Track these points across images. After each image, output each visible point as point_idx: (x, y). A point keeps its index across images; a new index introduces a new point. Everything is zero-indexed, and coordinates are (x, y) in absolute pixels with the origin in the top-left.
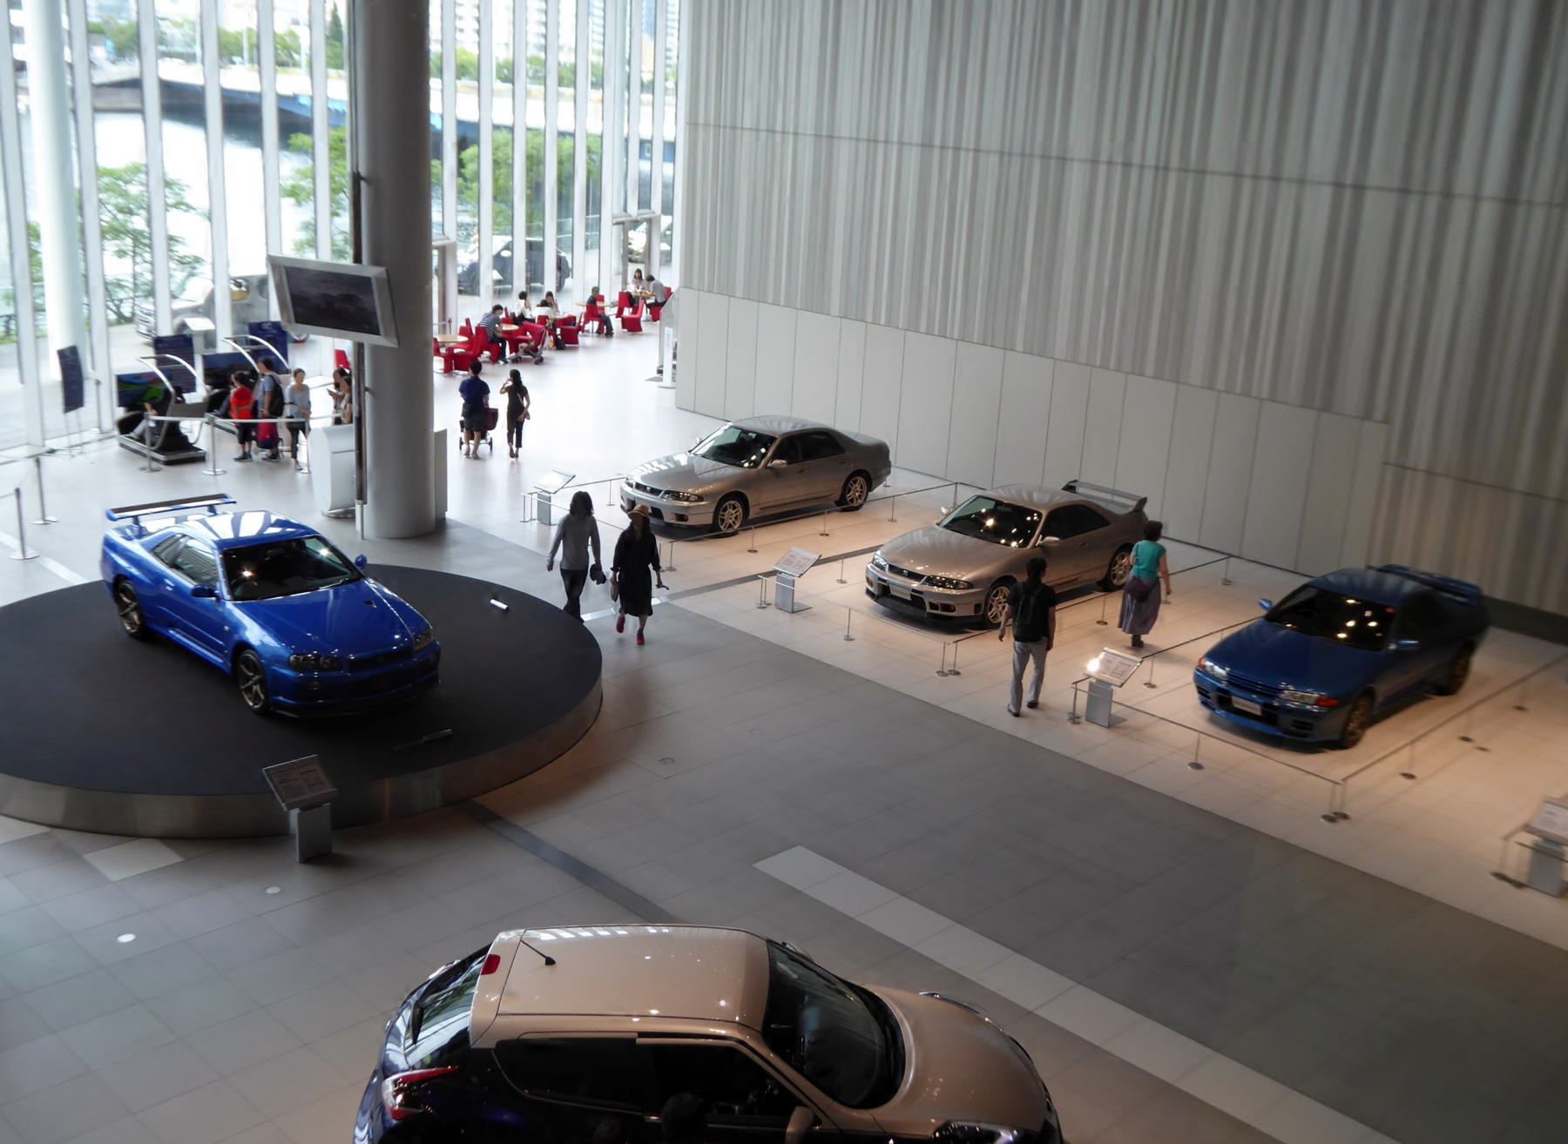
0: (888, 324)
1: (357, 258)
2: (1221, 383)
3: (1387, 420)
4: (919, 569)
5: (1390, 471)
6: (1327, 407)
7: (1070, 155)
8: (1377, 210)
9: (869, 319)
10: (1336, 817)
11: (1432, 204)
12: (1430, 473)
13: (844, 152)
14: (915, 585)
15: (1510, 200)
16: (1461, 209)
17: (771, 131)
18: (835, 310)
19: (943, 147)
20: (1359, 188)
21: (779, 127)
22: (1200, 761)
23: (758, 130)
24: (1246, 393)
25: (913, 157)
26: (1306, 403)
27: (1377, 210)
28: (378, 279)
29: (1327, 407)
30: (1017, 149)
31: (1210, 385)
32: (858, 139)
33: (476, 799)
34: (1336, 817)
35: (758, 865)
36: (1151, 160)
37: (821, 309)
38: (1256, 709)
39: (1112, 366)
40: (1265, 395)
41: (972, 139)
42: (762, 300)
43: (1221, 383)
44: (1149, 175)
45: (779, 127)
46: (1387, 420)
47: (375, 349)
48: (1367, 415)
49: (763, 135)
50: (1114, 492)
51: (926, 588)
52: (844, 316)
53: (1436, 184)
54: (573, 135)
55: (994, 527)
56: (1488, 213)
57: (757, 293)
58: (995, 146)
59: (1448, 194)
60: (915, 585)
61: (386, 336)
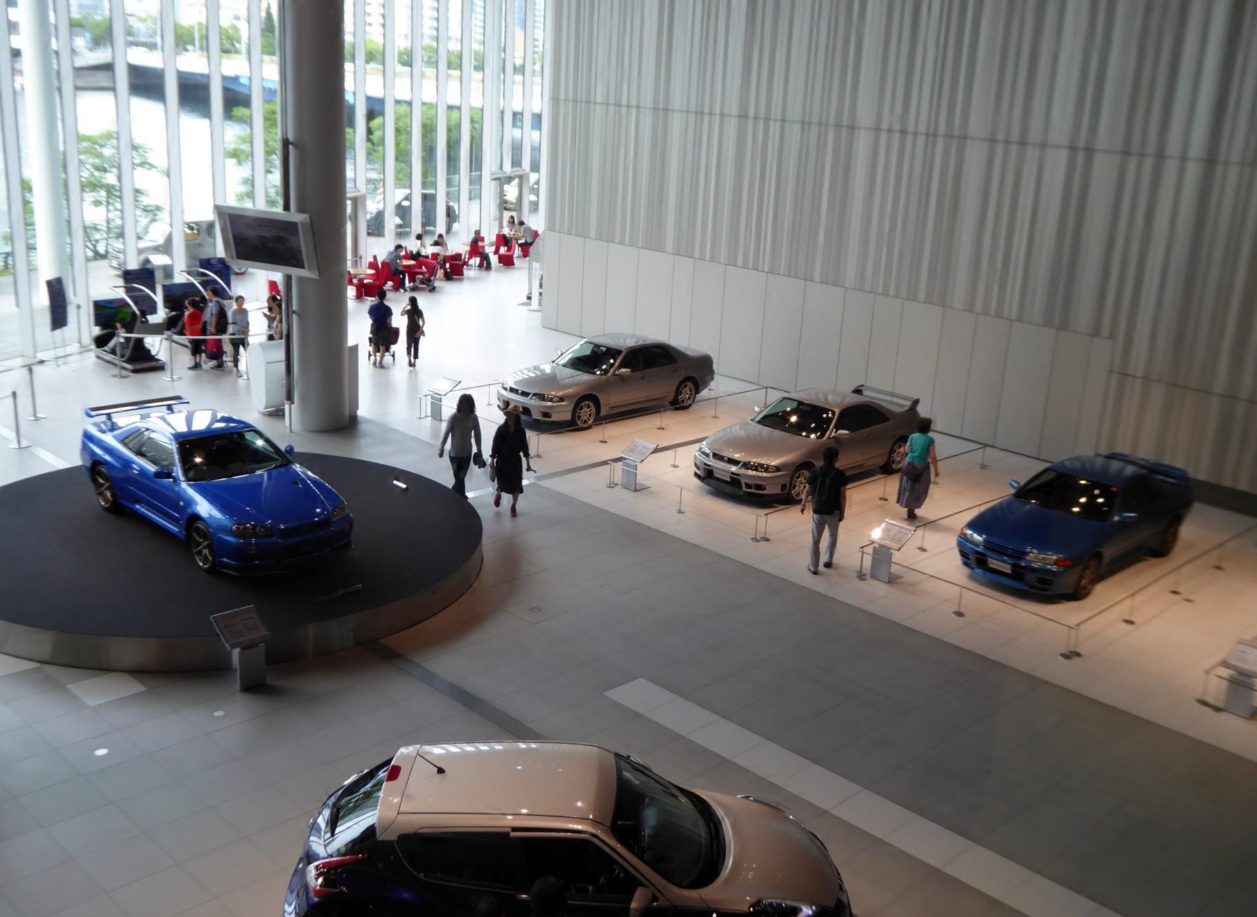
0: (712, 260)
1: (287, 207)
2: (979, 307)
3: (1112, 337)
4: (737, 456)
5: (1114, 377)
6: (1064, 326)
7: (857, 125)
8: (1104, 169)
9: (697, 256)
10: (1071, 655)
11: (1148, 164)
12: (1146, 379)
13: (676, 122)
14: (734, 469)
15: (1210, 160)
16: (1171, 168)
17: (618, 105)
18: (669, 248)
19: (756, 118)
20: (1090, 151)
21: (624, 102)
22: (962, 610)
23: (607, 104)
24: (999, 315)
25: (732, 126)
26: (1047, 323)
27: (1104, 169)
28: (303, 224)
29: (1064, 326)
30: (815, 119)
31: (970, 309)
32: (687, 112)
33: (381, 641)
34: (1071, 655)
35: (607, 694)
36: (922, 128)
37: (658, 247)
38: (1007, 569)
39: (891, 293)
40: (1014, 316)
41: (780, 111)
42: (610, 240)
43: (979, 307)
44: (921, 140)
45: (624, 102)
46: (1112, 337)
47: (301, 280)
48: (1096, 333)
49: (612, 109)
50: (893, 395)
51: (743, 471)
52: (677, 253)
53: (1151, 147)
54: (459, 108)
55: (797, 422)
56: (1193, 171)
57: (607, 235)
58: (798, 117)
59: (1160, 156)
60: (734, 469)
61: (309, 269)
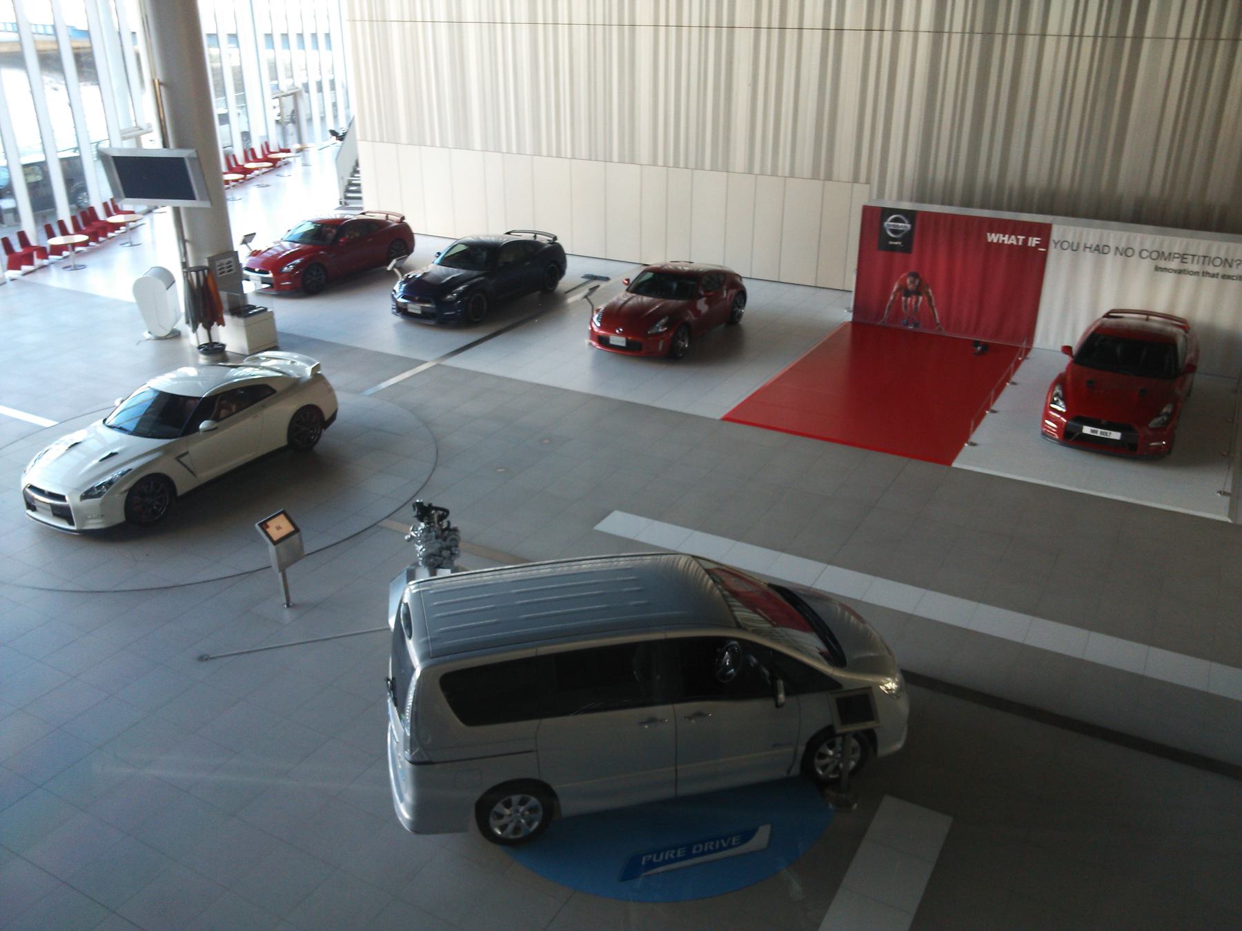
0: (442, 146)
1: (165, 145)
2: (757, 169)
3: (868, 182)
6: (829, 177)
8: (852, 45)
11: (888, 36)
13: (471, 32)
15: (938, 32)
16: (906, 40)
17: (679, 26)
19: (718, 27)
20: (1072, 36)
21: (540, 20)
24: (774, 174)
25: (524, 32)
26: (815, 175)
27: (852, 45)
28: (191, 159)
29: (829, 177)
30: (600, 20)
31: (750, 171)
33: (600, 527)
35: (600, 527)
36: (695, 22)
37: (468, 146)
39: (682, 165)
40: (787, 174)
41: (796, 19)
42: (422, 143)
43: (757, 169)
44: (695, 31)
46: (868, 182)
47: (188, 209)
48: (856, 180)
52: (485, 150)
53: (888, 25)
54: (216, 35)
56: (924, 41)
58: (583, 20)
59: (897, 30)
61: (202, 199)
